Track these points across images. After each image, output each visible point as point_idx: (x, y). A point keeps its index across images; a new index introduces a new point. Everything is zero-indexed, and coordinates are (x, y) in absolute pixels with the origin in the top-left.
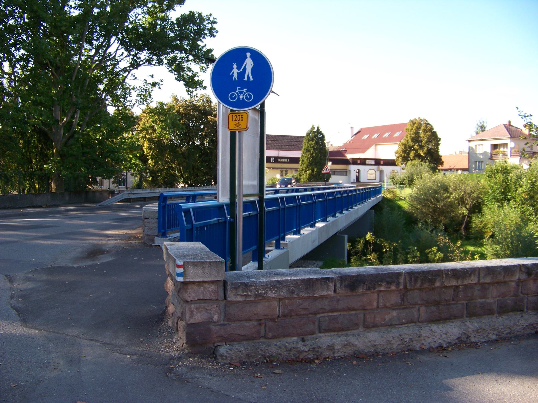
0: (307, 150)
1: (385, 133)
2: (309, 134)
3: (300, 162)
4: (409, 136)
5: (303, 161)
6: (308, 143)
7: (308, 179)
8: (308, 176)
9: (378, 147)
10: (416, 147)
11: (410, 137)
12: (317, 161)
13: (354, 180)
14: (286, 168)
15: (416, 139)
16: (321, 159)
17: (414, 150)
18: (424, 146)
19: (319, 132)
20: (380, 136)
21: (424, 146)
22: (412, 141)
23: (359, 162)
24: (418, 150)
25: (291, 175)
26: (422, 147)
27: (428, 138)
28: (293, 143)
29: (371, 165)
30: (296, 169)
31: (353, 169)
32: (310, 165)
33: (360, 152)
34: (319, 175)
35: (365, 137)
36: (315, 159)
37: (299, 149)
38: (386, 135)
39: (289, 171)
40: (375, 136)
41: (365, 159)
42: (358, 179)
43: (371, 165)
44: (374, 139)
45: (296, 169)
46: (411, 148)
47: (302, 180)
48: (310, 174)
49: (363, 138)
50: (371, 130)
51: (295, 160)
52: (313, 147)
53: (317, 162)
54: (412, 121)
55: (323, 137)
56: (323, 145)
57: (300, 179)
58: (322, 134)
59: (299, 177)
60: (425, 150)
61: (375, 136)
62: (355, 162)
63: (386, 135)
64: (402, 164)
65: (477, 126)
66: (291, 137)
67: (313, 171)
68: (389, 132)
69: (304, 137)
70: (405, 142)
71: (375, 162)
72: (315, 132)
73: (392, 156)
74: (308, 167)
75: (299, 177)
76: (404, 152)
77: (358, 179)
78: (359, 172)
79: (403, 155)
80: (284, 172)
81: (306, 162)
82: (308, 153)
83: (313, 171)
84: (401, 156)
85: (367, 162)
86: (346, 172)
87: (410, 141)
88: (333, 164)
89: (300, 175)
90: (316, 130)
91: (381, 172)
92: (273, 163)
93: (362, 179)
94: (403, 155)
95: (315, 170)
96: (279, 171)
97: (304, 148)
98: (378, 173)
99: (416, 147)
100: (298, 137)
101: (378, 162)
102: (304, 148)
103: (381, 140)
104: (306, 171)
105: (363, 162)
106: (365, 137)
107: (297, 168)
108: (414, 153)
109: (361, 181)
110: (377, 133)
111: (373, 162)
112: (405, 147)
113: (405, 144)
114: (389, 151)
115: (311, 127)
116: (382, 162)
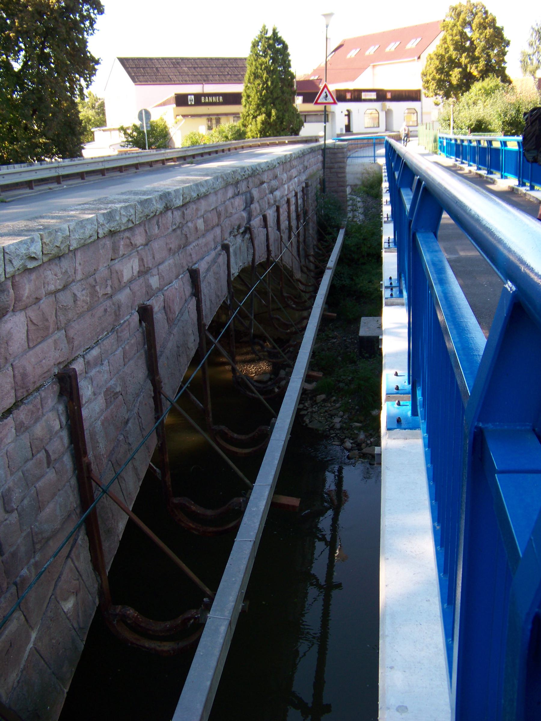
0: (256, 76)
1: (388, 44)
2: (258, 42)
3: (243, 100)
4: (449, 38)
5: (248, 97)
6: (256, 60)
7: (260, 132)
8: (259, 126)
9: (377, 69)
10: (464, 60)
11: (452, 40)
12: (275, 95)
13: (341, 130)
14: (217, 115)
15: (463, 45)
16: (283, 92)
17: (459, 65)
18: (478, 58)
19: (276, 38)
20: (381, 49)
21: (478, 58)
22: (455, 49)
23: (348, 96)
24: (466, 66)
25: (227, 124)
26: (474, 60)
27: (487, 41)
28: (227, 69)
29: (370, 100)
30: (236, 115)
31: (340, 109)
32: (263, 105)
33: (346, 81)
34: (282, 123)
35: (352, 54)
36: (272, 93)
37: (239, 81)
38: (392, 47)
39: (223, 120)
40: (371, 51)
41: (360, 91)
42: (348, 128)
43: (370, 100)
44: (369, 56)
45: (236, 115)
46: (453, 63)
47: (249, 134)
48: (263, 123)
49: (348, 56)
50: (363, 42)
51: (233, 99)
52: (266, 68)
53: (277, 98)
54: (454, 9)
55: (285, 47)
56: (286, 64)
57: (245, 133)
58: (283, 43)
59: (242, 129)
60: (482, 63)
61: (371, 51)
62: (341, 97)
63: (392, 47)
64: (436, 94)
65: (531, 31)
66: (223, 59)
67: (269, 115)
68: (395, 41)
69: (245, 59)
70: (442, 52)
71: (378, 95)
72: (269, 39)
73: (414, 83)
74: (258, 107)
75: (242, 129)
76: (440, 70)
77: (348, 128)
78: (349, 115)
79: (438, 77)
80: (214, 122)
81: (255, 99)
82: (258, 81)
83: (269, 115)
84: (433, 79)
85: (364, 96)
86: (325, 116)
87: (452, 48)
88: (305, 101)
89: (245, 126)
90: (270, 34)
91: (388, 113)
92: (191, 105)
93: (355, 128)
94: (438, 77)
95: (273, 112)
96: (204, 120)
97: (248, 72)
98: (383, 115)
99: (464, 60)
100: (236, 60)
101: (381, 96)
102: (248, 72)
103: (382, 56)
104: (255, 117)
105: (356, 96)
106: (352, 54)
107: (238, 114)
108: (460, 73)
109: (354, 132)
110: (374, 45)
111: (373, 96)
112: (441, 62)
113: (443, 56)
114: (408, 75)
115: (260, 28)
116: (389, 96)
